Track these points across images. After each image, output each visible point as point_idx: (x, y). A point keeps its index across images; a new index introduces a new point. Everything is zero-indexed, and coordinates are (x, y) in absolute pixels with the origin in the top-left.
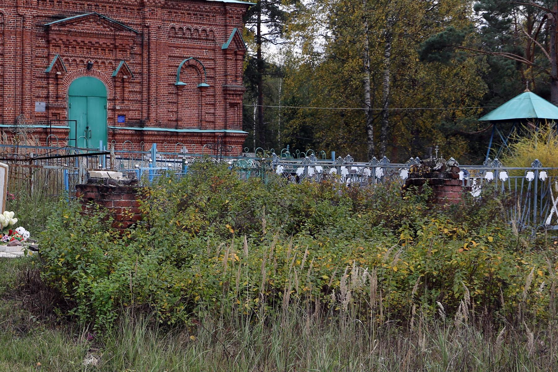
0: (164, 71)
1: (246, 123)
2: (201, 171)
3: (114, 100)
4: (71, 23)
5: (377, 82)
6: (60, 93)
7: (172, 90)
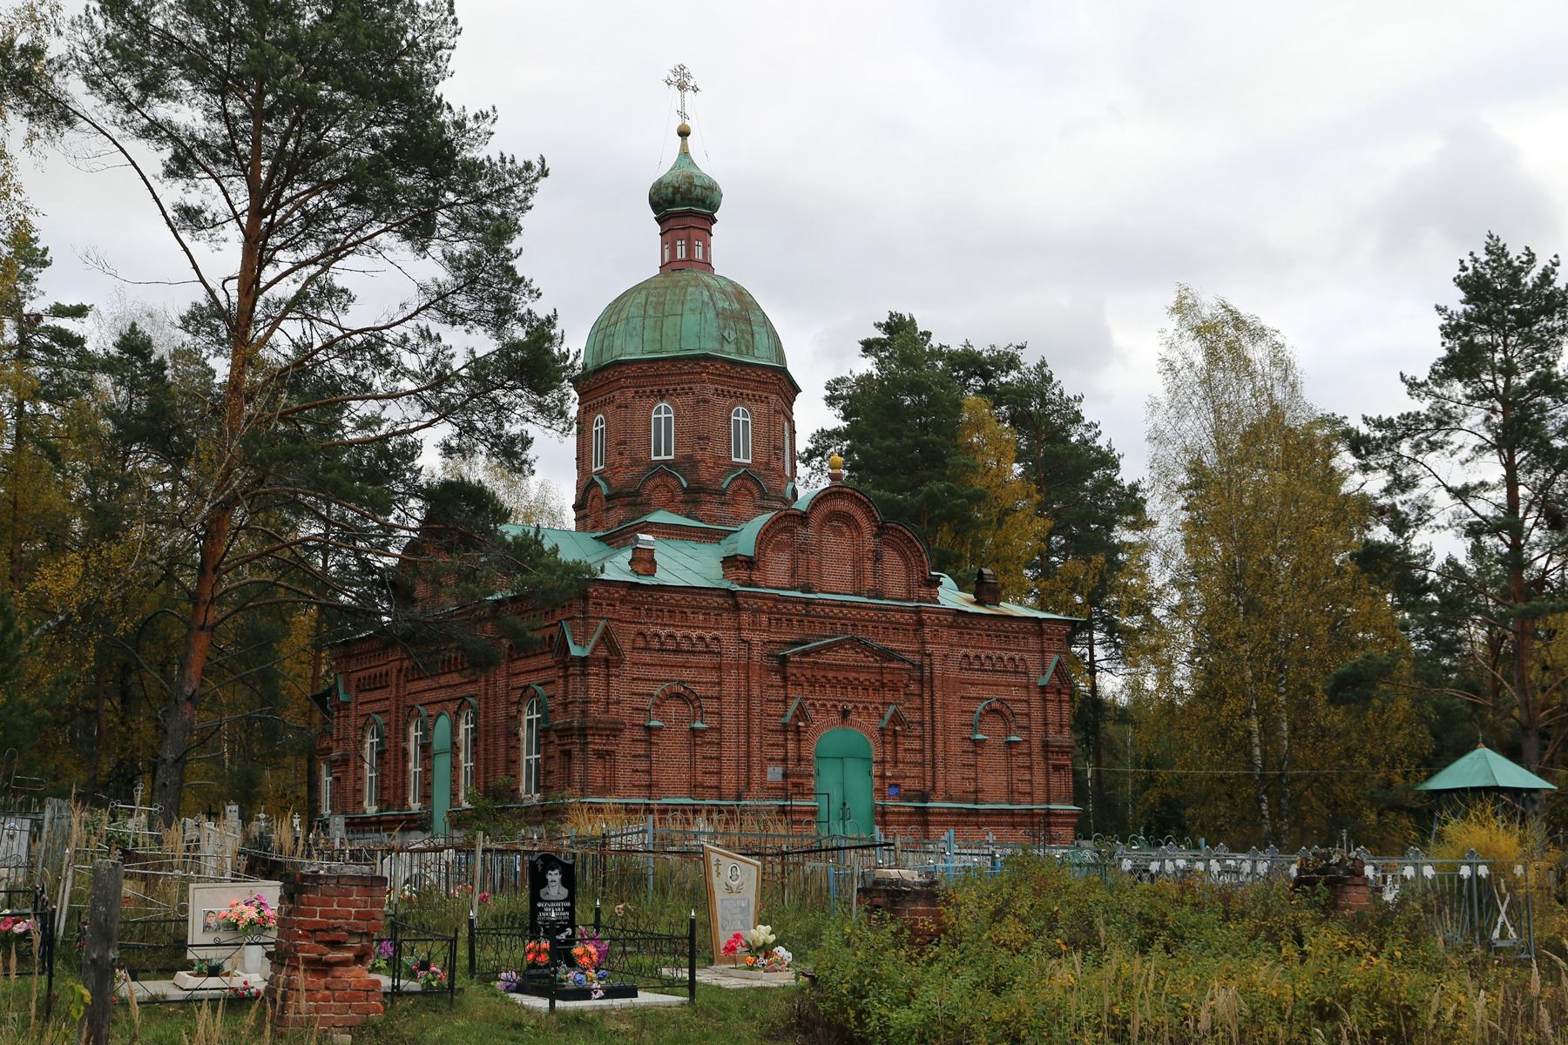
0: (955, 719)
1: (1079, 796)
2: (1020, 868)
3: (883, 762)
4: (817, 650)
5: (1269, 730)
6: (804, 753)
7: (968, 746)
